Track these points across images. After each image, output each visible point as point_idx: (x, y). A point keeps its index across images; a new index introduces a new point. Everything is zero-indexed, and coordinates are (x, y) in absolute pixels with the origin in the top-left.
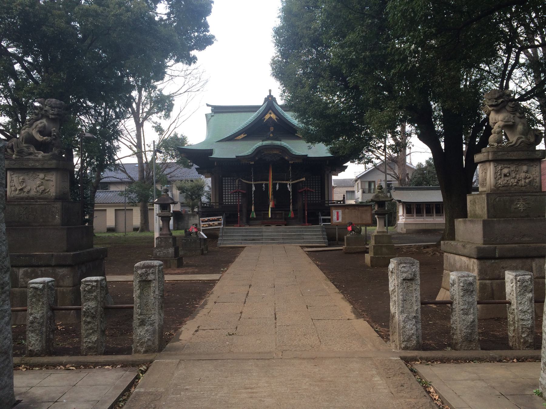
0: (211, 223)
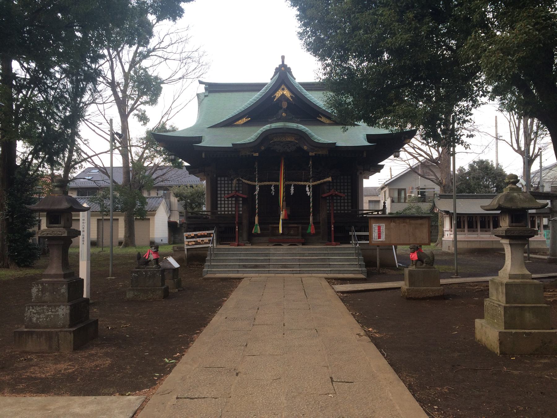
0: (199, 240)
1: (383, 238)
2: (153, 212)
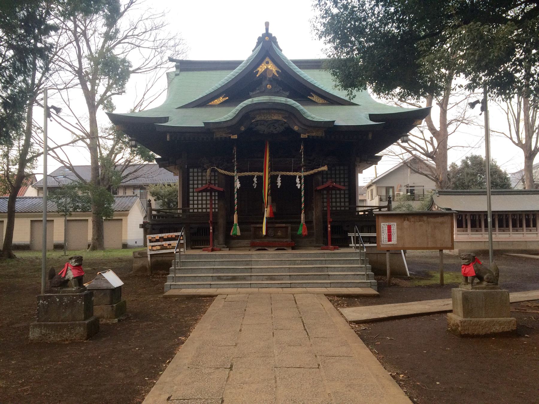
2: (125, 212)
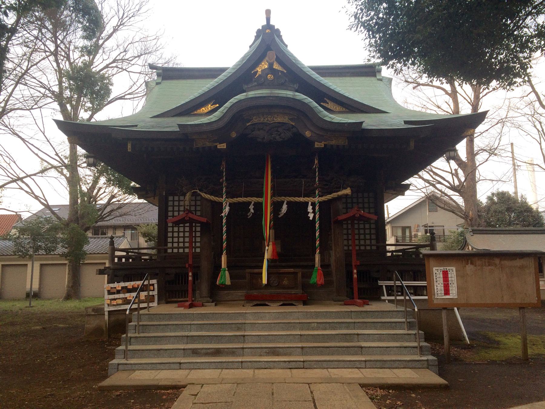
1: (454, 293)
